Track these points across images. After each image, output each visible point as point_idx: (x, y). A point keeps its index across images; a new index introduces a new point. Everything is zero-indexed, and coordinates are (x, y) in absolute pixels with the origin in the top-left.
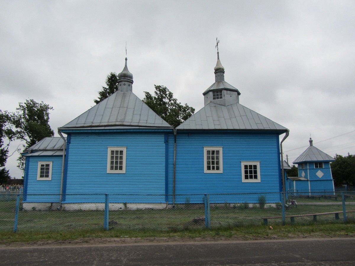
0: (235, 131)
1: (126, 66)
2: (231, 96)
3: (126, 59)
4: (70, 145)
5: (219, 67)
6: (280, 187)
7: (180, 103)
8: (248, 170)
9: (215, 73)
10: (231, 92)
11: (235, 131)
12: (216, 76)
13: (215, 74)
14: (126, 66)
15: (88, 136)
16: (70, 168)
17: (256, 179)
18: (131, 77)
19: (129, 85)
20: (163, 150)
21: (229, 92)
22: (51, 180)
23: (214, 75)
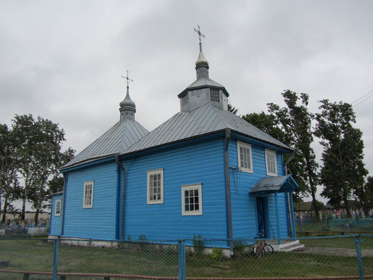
0: (168, 146)
1: (128, 95)
2: (198, 96)
3: (128, 88)
4: (68, 183)
5: (201, 60)
6: (116, 221)
7: (336, 102)
8: (194, 197)
9: (197, 69)
10: (199, 91)
11: (168, 146)
12: (197, 73)
13: (196, 69)
14: (128, 95)
15: (75, 174)
16: (67, 204)
17: (196, 211)
18: (134, 106)
19: (132, 114)
20: (115, 180)
21: (195, 92)
22: (202, 214)
23: (195, 71)
